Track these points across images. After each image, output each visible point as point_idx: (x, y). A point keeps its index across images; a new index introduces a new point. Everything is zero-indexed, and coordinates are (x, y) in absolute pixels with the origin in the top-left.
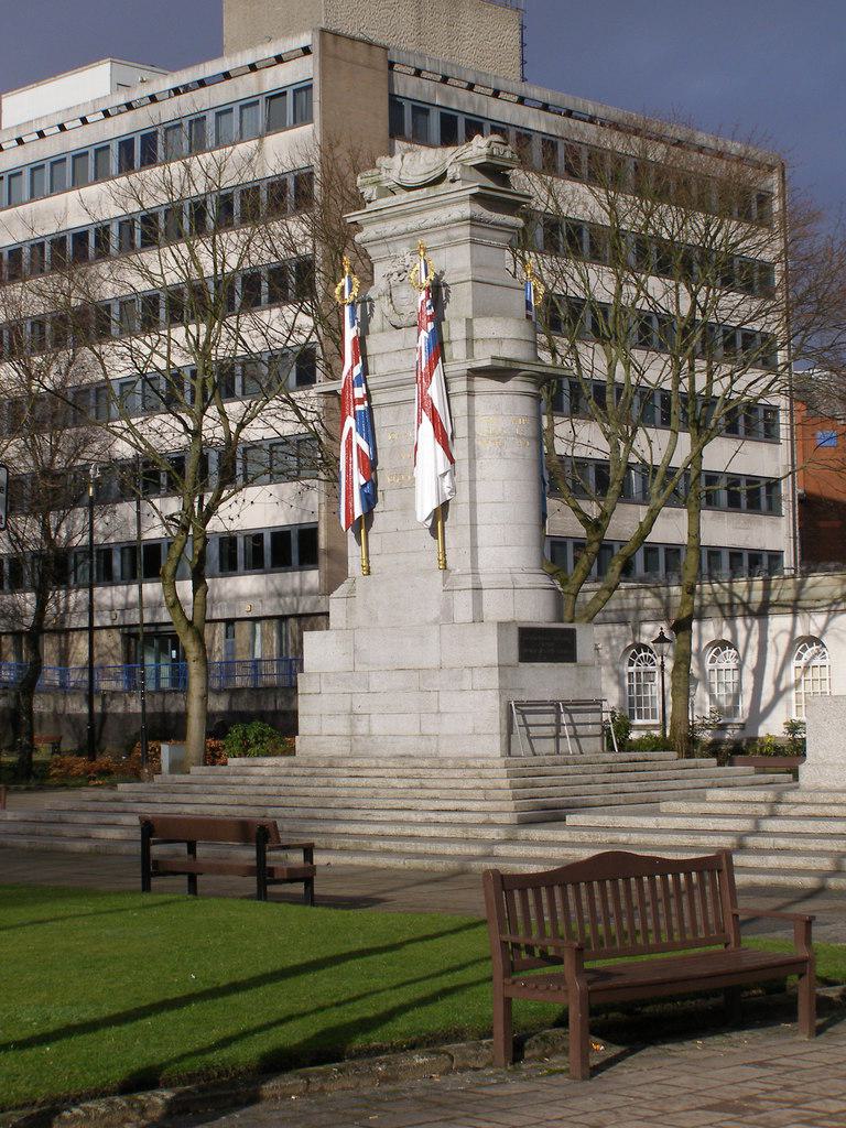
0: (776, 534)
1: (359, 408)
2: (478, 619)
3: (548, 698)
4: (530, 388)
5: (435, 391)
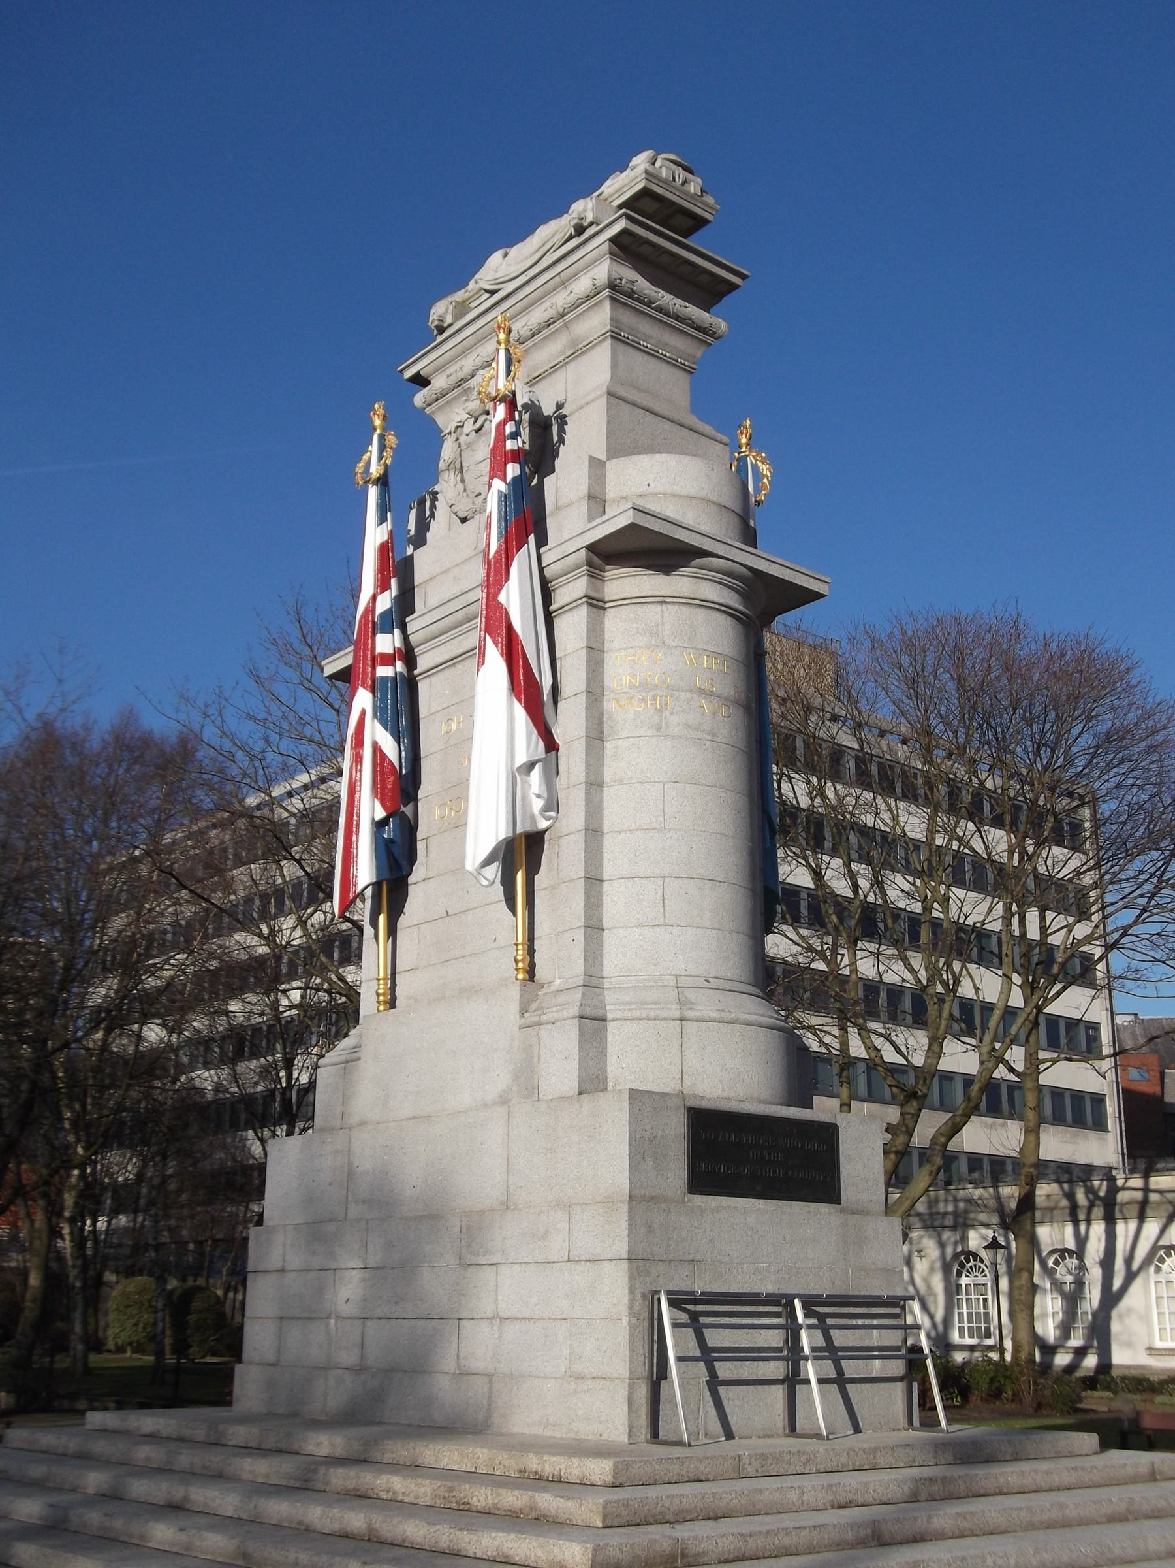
0: (1103, 1149)
1: (383, 671)
2: (592, 1082)
3: (767, 1287)
4: (732, 599)
5: (516, 598)
